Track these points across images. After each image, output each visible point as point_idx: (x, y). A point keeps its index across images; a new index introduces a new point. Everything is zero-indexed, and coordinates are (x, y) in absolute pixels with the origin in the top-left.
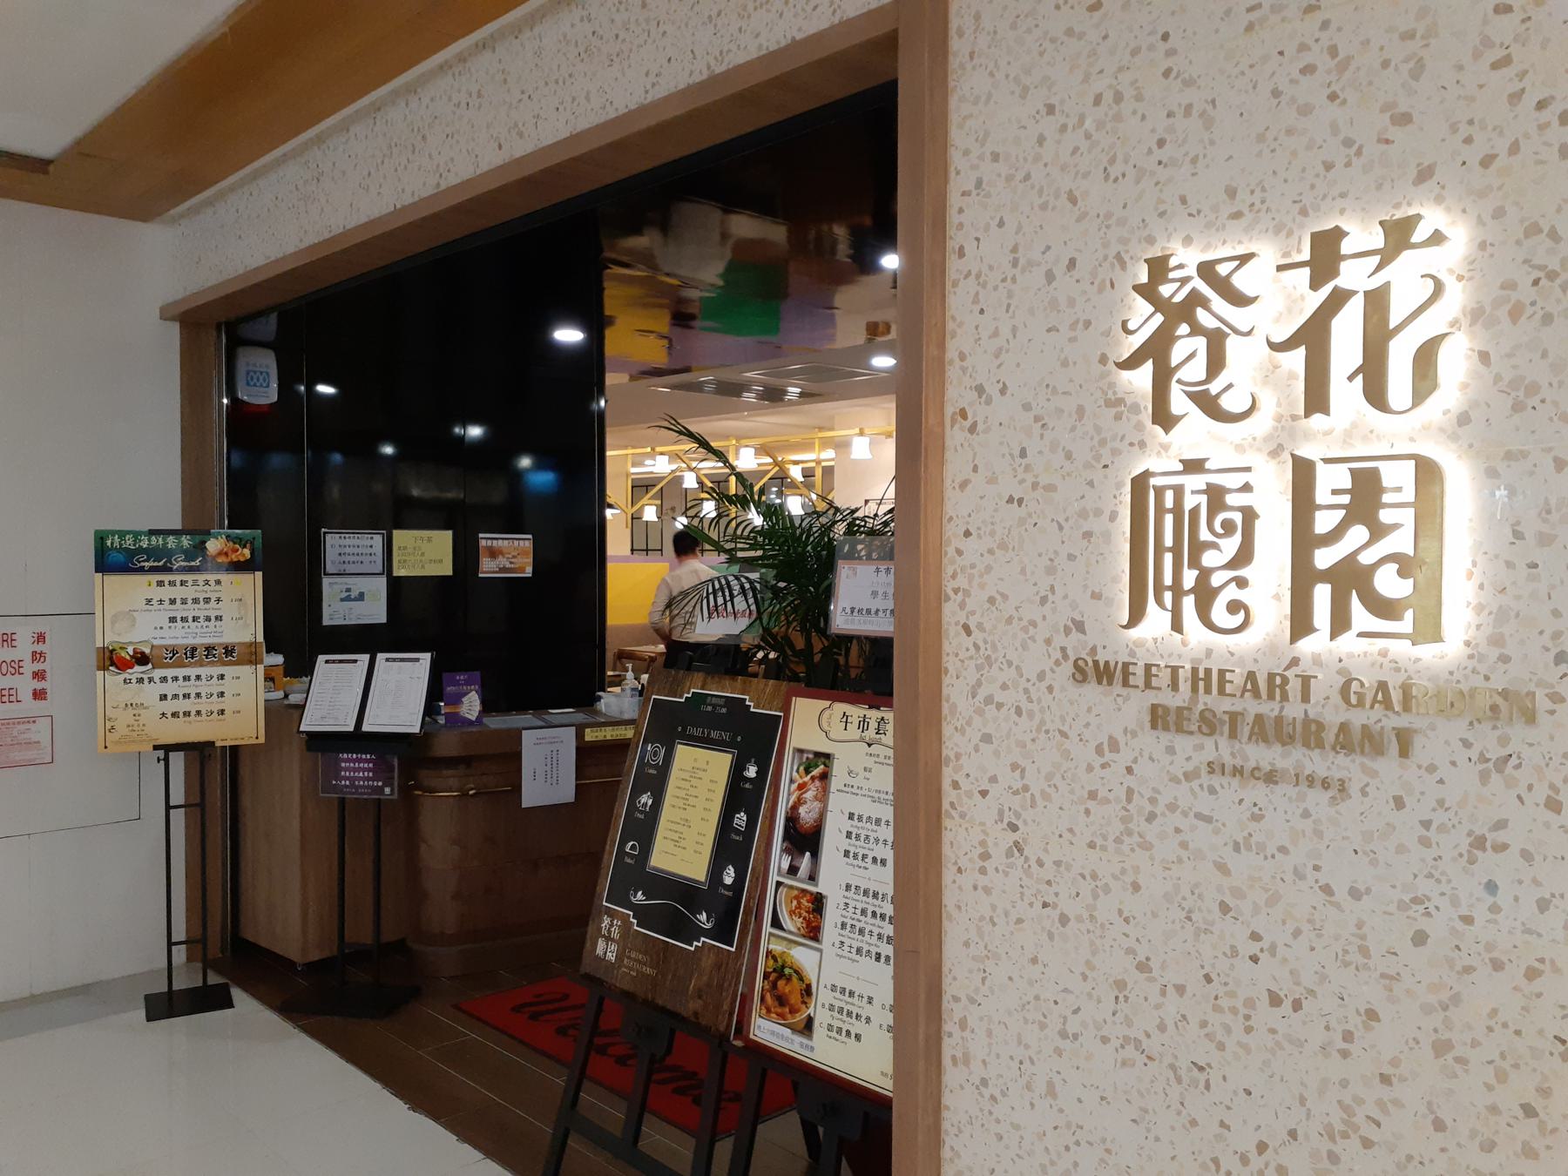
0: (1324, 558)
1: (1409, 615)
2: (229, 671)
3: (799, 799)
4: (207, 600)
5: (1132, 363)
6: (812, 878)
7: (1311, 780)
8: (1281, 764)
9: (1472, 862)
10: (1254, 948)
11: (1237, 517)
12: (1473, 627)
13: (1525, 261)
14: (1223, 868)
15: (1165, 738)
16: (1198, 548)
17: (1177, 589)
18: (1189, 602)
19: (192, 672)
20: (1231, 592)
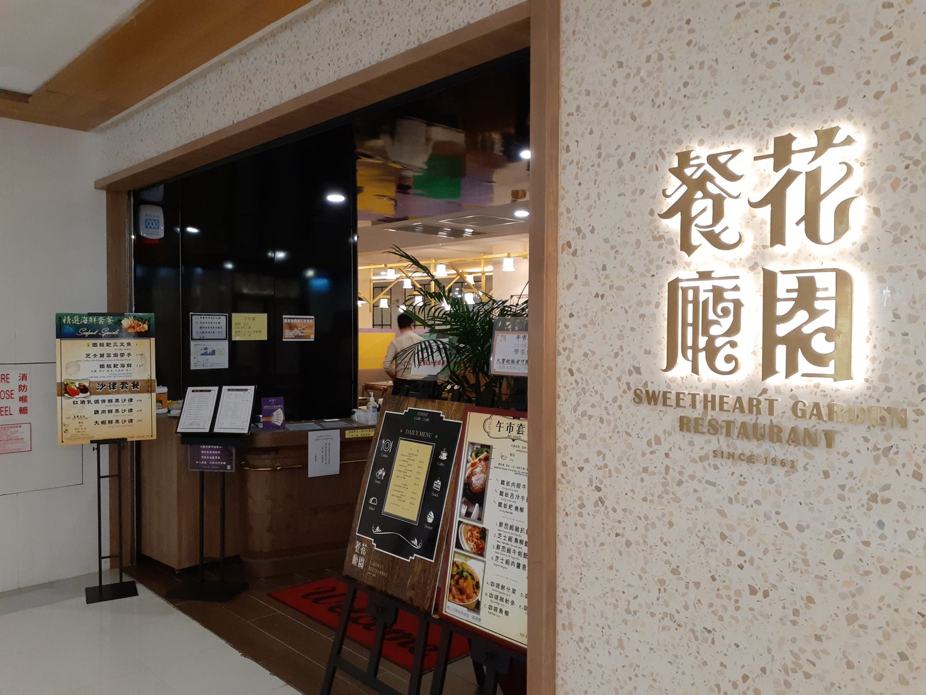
0: (782, 330)
1: (832, 363)
2: (135, 397)
3: (472, 472)
4: (122, 355)
5: (669, 214)
6: (480, 519)
7: (774, 461)
8: (756, 451)
9: (869, 509)
10: (741, 560)
11: (731, 306)
12: (870, 371)
13: (901, 155)
14: (722, 513)
15: (688, 436)
16: (707, 324)
17: (695, 348)
18: (702, 356)
19: (113, 397)
20: (727, 350)
